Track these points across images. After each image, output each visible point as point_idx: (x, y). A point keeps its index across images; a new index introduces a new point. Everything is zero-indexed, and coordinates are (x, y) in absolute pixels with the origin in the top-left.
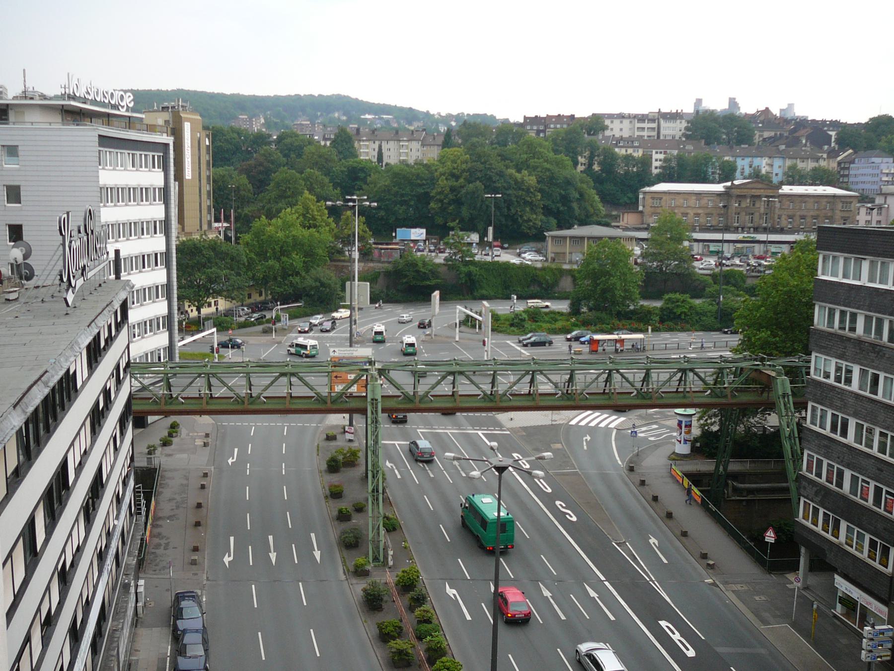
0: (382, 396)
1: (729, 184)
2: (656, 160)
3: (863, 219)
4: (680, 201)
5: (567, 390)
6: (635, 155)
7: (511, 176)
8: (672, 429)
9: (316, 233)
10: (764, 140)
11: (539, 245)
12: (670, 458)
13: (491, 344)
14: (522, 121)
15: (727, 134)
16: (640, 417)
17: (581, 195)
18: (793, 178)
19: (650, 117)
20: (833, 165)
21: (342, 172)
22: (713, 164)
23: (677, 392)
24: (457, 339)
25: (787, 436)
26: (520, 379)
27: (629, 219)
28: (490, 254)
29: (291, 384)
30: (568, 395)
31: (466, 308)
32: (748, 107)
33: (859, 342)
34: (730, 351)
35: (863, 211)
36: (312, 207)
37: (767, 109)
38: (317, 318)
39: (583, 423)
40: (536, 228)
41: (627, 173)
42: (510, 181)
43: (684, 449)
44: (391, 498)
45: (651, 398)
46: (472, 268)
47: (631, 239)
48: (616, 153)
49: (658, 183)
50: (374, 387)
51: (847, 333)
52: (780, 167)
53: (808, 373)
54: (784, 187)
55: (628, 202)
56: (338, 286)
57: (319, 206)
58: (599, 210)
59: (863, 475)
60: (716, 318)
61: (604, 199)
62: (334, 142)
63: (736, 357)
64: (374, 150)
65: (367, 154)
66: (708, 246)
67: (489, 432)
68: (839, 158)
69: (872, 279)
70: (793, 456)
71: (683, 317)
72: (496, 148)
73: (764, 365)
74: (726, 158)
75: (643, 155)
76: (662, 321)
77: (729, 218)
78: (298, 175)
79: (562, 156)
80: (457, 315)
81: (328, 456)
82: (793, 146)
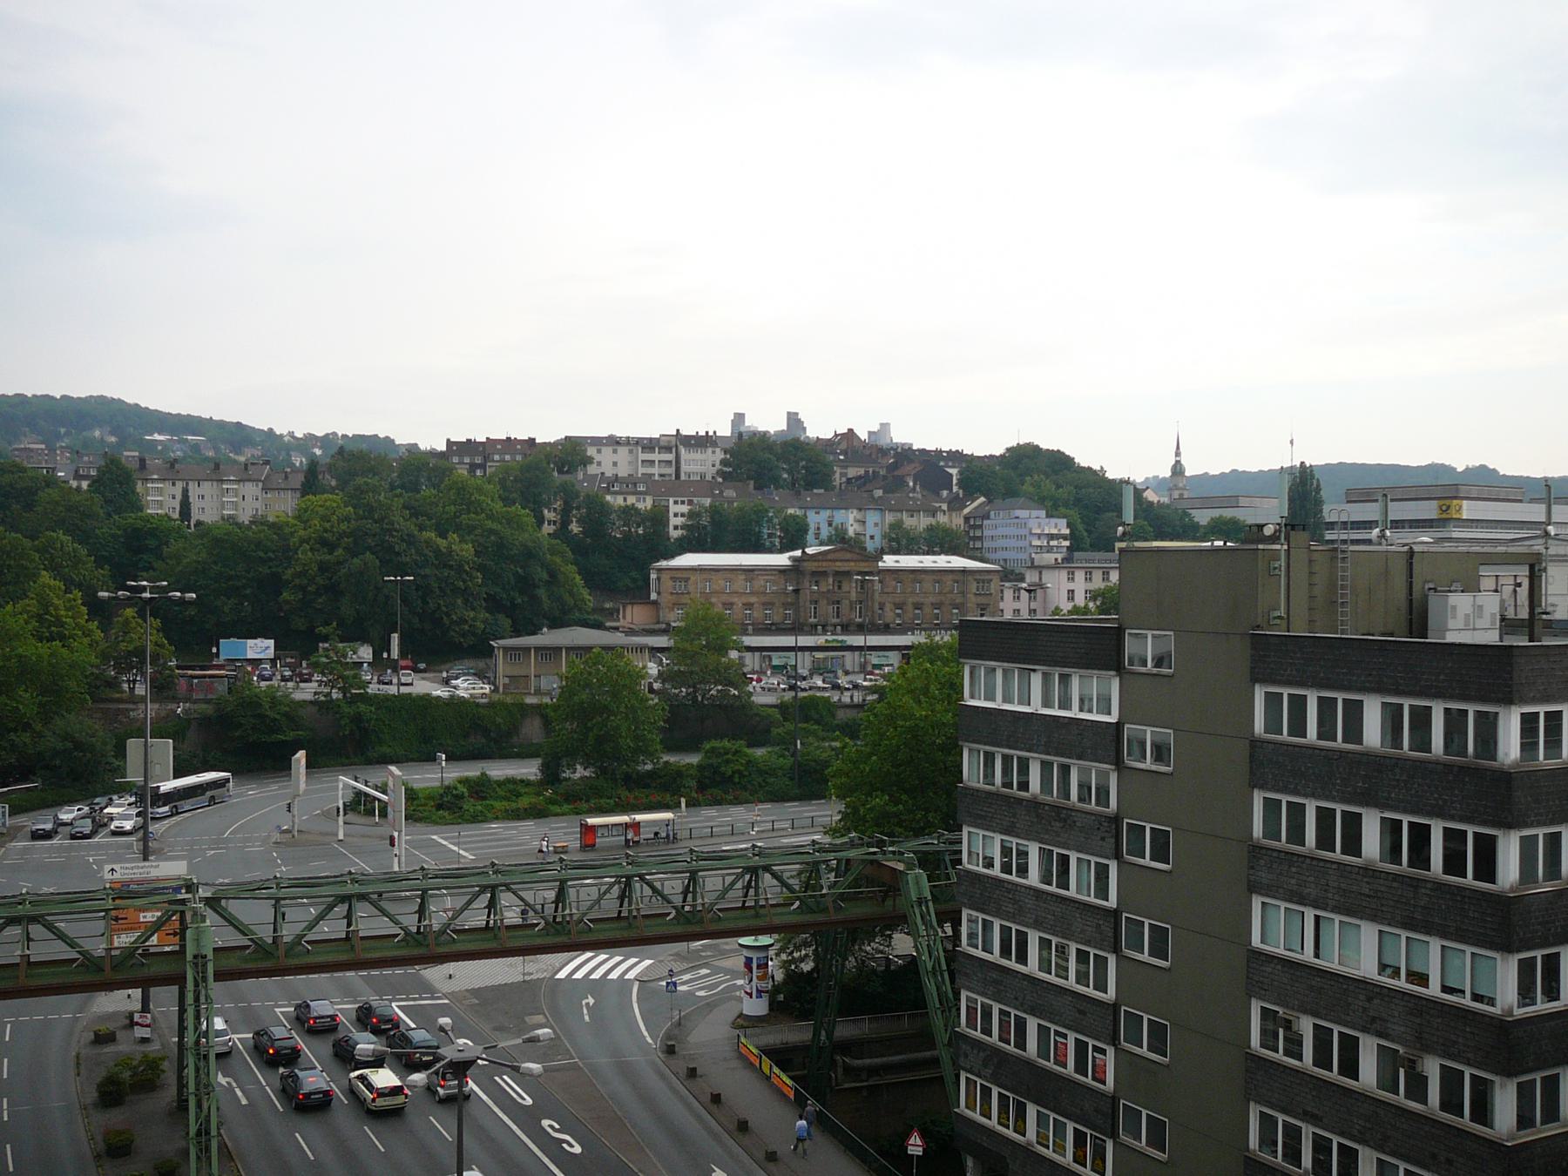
0: (215, 949)
1: (798, 553)
2: (676, 515)
3: (1012, 607)
4: (719, 583)
5: (555, 917)
6: (640, 506)
7: (428, 542)
8: (734, 974)
9: (64, 651)
10: (849, 481)
11: (481, 664)
12: (735, 1025)
13: (406, 842)
14: (442, 447)
15: (789, 472)
16: (678, 956)
17: (552, 574)
18: (898, 543)
19: (662, 444)
20: (957, 521)
21: (113, 536)
22: (770, 520)
23: (743, 907)
24: (341, 837)
25: (930, 969)
26: (470, 902)
27: (635, 615)
28: (395, 681)
29: (29, 939)
30: (555, 926)
31: (356, 779)
32: (819, 428)
33: (1034, 804)
34: (825, 833)
35: (1008, 594)
36: (56, 601)
37: (851, 431)
38: (73, 811)
39: (579, 975)
40: (474, 634)
41: (627, 536)
42: (426, 551)
43: (756, 1007)
44: (229, 1144)
45: (701, 921)
46: (362, 707)
47: (641, 649)
48: (608, 502)
49: (680, 554)
50: (199, 931)
51: (1015, 791)
52: (876, 525)
53: (960, 862)
54: (886, 557)
55: (632, 586)
56: (109, 747)
57: (69, 601)
58: (583, 600)
59: (1056, 1023)
60: (792, 779)
61: (591, 579)
62: (96, 483)
63: (838, 841)
64: (174, 498)
65: (160, 504)
66: (770, 659)
67: (412, 1003)
68: (966, 511)
69: (1047, 703)
70: (941, 1003)
71: (737, 780)
72: (401, 495)
73: (884, 853)
74: (791, 511)
75: (654, 506)
76: (702, 788)
77: (802, 609)
78: (27, 543)
79: (517, 509)
80: (340, 793)
81: (101, 1075)
82: (893, 492)
